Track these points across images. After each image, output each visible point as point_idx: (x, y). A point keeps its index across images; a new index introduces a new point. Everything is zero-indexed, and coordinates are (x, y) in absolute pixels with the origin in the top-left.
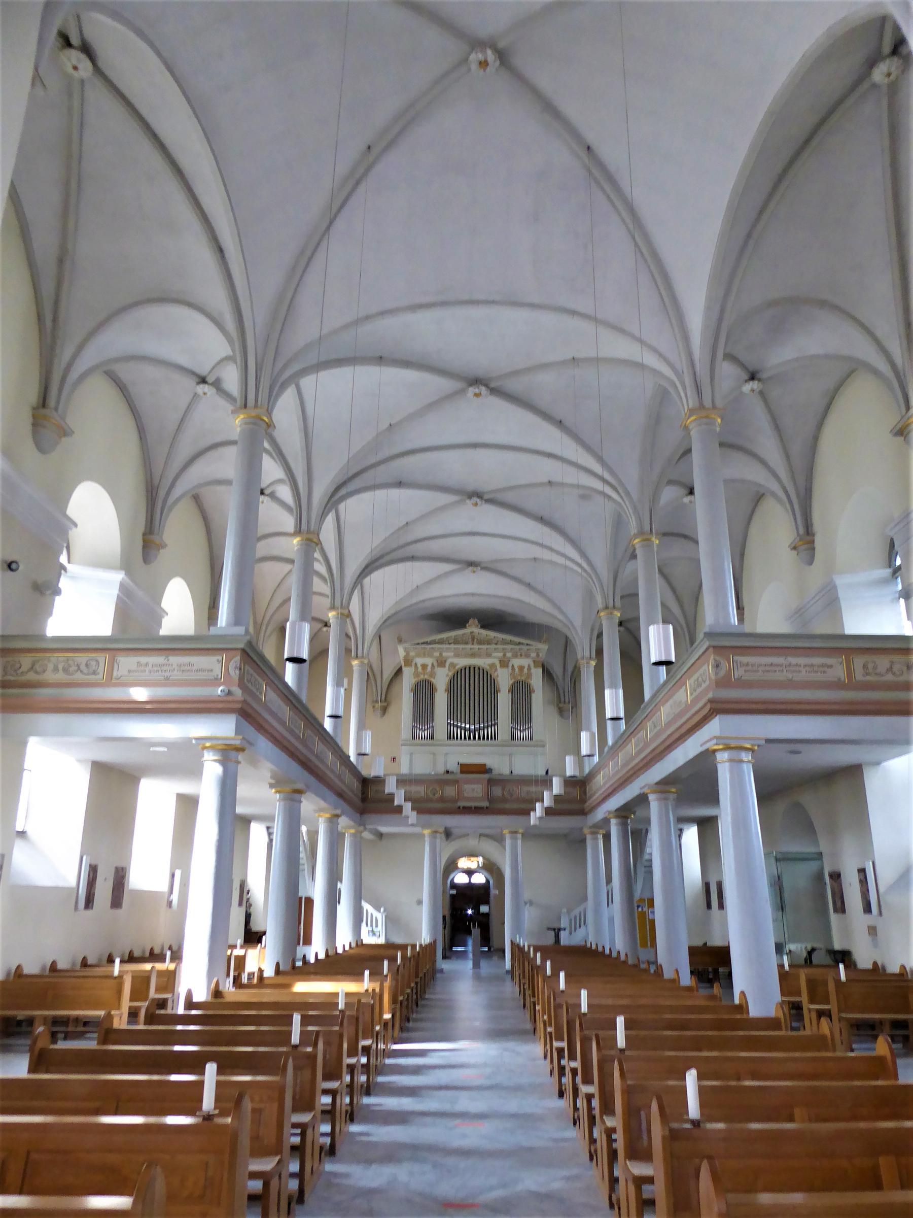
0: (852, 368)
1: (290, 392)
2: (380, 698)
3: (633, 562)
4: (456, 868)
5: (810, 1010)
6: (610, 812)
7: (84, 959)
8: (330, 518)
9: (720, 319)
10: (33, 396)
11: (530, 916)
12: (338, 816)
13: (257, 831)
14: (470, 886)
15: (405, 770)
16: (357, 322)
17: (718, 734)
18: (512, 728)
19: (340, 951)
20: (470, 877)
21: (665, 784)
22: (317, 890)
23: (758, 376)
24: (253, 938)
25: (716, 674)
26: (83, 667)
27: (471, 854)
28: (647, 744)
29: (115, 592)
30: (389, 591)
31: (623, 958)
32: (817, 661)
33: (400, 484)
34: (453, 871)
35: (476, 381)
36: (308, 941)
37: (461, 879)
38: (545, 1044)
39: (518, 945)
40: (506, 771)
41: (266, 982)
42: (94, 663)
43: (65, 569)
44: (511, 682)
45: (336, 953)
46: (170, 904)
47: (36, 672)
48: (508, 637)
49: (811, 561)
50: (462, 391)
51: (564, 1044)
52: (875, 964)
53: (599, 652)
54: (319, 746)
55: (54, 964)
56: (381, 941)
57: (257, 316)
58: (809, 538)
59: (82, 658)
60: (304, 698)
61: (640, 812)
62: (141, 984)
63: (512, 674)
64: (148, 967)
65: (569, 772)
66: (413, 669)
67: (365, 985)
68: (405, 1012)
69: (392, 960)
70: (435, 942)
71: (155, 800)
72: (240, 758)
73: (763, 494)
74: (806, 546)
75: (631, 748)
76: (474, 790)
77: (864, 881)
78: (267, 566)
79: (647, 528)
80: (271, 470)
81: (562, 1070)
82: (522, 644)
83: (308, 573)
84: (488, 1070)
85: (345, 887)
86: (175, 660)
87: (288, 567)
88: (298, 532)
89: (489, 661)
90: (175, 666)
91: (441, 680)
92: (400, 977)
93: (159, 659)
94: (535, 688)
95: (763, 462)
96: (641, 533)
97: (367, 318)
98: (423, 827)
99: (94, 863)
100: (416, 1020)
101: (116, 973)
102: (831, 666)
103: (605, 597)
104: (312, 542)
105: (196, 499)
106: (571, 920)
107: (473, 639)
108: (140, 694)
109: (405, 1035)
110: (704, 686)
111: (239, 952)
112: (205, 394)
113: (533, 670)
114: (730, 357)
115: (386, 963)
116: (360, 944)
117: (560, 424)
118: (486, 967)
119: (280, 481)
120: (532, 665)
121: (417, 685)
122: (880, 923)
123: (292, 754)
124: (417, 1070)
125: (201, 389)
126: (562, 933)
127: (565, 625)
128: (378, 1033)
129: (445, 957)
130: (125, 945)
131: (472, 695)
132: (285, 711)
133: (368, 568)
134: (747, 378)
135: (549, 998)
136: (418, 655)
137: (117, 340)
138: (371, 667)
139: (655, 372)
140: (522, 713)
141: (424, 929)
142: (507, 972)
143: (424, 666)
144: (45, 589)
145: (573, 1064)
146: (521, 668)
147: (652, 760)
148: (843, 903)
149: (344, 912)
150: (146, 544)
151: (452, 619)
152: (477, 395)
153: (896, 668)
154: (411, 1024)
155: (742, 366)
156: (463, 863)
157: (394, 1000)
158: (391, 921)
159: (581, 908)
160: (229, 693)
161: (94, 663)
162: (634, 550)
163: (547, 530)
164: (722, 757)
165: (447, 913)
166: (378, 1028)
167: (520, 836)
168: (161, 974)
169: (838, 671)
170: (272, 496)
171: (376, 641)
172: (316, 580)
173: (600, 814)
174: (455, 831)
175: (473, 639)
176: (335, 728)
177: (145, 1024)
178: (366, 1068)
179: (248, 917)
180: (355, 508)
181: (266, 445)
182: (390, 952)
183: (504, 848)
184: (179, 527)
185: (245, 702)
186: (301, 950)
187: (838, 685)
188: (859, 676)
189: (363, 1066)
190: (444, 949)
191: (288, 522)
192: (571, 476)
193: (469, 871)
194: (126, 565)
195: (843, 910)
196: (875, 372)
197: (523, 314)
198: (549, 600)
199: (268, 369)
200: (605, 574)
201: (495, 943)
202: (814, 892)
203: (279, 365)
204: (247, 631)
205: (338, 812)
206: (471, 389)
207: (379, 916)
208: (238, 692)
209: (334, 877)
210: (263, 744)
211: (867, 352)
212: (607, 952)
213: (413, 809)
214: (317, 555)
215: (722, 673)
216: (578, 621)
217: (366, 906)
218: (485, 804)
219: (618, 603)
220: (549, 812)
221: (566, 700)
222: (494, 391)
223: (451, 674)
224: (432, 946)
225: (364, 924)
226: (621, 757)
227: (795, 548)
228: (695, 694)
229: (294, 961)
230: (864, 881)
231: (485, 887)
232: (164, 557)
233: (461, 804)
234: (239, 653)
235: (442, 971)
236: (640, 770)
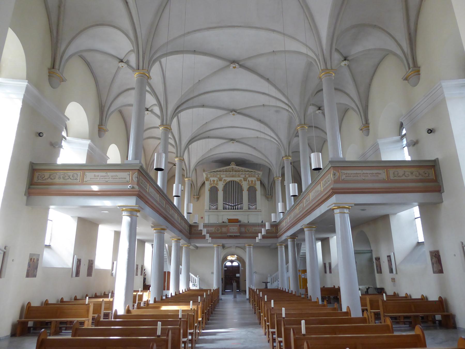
0: (387, 53)
1: (157, 65)
2: (196, 194)
3: (296, 138)
4: (227, 259)
5: (371, 312)
6: (288, 236)
7: (76, 296)
8: (175, 120)
9: (335, 29)
10: (48, 64)
11: (256, 278)
12: (180, 240)
13: (148, 247)
14: (232, 267)
15: (206, 222)
16: (184, 35)
17: (335, 202)
19: (181, 292)
20: (232, 263)
21: (311, 225)
22: (172, 269)
23: (348, 59)
24: (146, 287)
25: (334, 178)
26: (71, 177)
27: (232, 255)
28: (304, 209)
29: (87, 148)
30: (199, 151)
31: (294, 293)
32: (375, 171)
33: (203, 106)
34: (225, 261)
35: (234, 62)
36: (168, 289)
37: (229, 264)
38: (266, 329)
39: (252, 289)
40: (246, 221)
41: (150, 306)
42: (75, 175)
43: (65, 139)
44: (248, 187)
45: (180, 293)
46: (112, 274)
47: (51, 179)
48: (247, 169)
49: (368, 135)
50: (228, 66)
51: (275, 330)
52: (395, 293)
53: (283, 175)
54: (172, 212)
55: (62, 299)
56: (198, 288)
57: (143, 32)
58: (367, 125)
59: (70, 173)
60: (165, 192)
61: (300, 237)
62: (97, 308)
63: (249, 184)
64: (101, 300)
65: (273, 220)
66: (209, 182)
67: (191, 306)
68: (207, 317)
69: (202, 296)
70: (219, 288)
71: (105, 233)
72: (138, 214)
73: (348, 109)
75: (297, 211)
76: (234, 229)
78: (151, 141)
80: (150, 100)
81: (274, 340)
83: (166, 143)
84: (242, 341)
85: (183, 267)
86: (110, 174)
87: (158, 141)
88: (162, 124)
89: (239, 179)
90: (110, 177)
91: (220, 186)
92: (205, 303)
93: (103, 174)
95: (348, 95)
96: (300, 124)
97: (189, 33)
98: (214, 244)
99: (79, 258)
100: (212, 320)
101: (87, 303)
102: (380, 174)
103: (285, 152)
104: (167, 128)
105: (121, 112)
107: (233, 170)
108: (95, 188)
109: (207, 326)
110: (329, 183)
111: (140, 293)
112: (122, 67)
113: (257, 182)
114: (337, 50)
115: (199, 297)
116: (189, 290)
117: (268, 80)
118: (239, 298)
119: (155, 105)
121: (211, 188)
123: (160, 214)
124: (212, 341)
125: (121, 64)
126: (268, 284)
127: (269, 164)
128: (196, 326)
129: (222, 294)
130: (92, 292)
131: (233, 193)
132: (157, 197)
133: (191, 141)
134: (343, 59)
135: (267, 310)
136: (211, 177)
137: (83, 42)
138: (192, 181)
139: (307, 55)
140: (252, 199)
141: (214, 283)
142: (247, 299)
143: (214, 181)
144: (55, 146)
145: (280, 339)
146: (252, 181)
147: (305, 215)
149: (182, 278)
150: (99, 129)
151: (224, 162)
152: (234, 67)
154: (210, 321)
155: (341, 54)
156: (229, 258)
157: (203, 312)
158: (202, 280)
159: (275, 274)
160: (133, 188)
161: (75, 175)
162: (298, 132)
163: (262, 125)
164: (337, 211)
165: (223, 277)
166: (196, 324)
167: (252, 247)
168: (106, 303)
170: (152, 111)
171: (194, 172)
172: (170, 146)
173: (284, 237)
174: (226, 245)
175: (233, 170)
176: (178, 202)
178: (191, 341)
179: (145, 279)
180: (185, 115)
181: (148, 88)
182: (201, 293)
183: (246, 252)
184: (113, 123)
185: (139, 191)
186: (165, 292)
187: (383, 181)
189: (190, 340)
190: (222, 291)
191: (158, 122)
192: (273, 102)
193: (232, 261)
194: (91, 137)
196: (395, 54)
197: (252, 32)
199: (148, 54)
200: (285, 142)
201: (242, 288)
202: (370, 266)
203: (153, 52)
204: (140, 162)
205: (180, 238)
206: (232, 65)
207: (197, 279)
208: (137, 188)
209: (178, 263)
210: (148, 210)
211: (393, 47)
212: (287, 291)
213: (210, 237)
214: (170, 136)
215: (336, 177)
216: (274, 162)
217: (191, 275)
218: (239, 234)
219: (291, 154)
220: (264, 237)
221: (269, 194)
222: (241, 66)
223: (224, 184)
224: (218, 290)
225: (191, 282)
226: (292, 215)
227: (361, 130)
228: (325, 187)
229: (162, 297)
231: (238, 267)
232: (108, 135)
233: (229, 235)
234: (137, 171)
235: (221, 300)
236: (300, 219)
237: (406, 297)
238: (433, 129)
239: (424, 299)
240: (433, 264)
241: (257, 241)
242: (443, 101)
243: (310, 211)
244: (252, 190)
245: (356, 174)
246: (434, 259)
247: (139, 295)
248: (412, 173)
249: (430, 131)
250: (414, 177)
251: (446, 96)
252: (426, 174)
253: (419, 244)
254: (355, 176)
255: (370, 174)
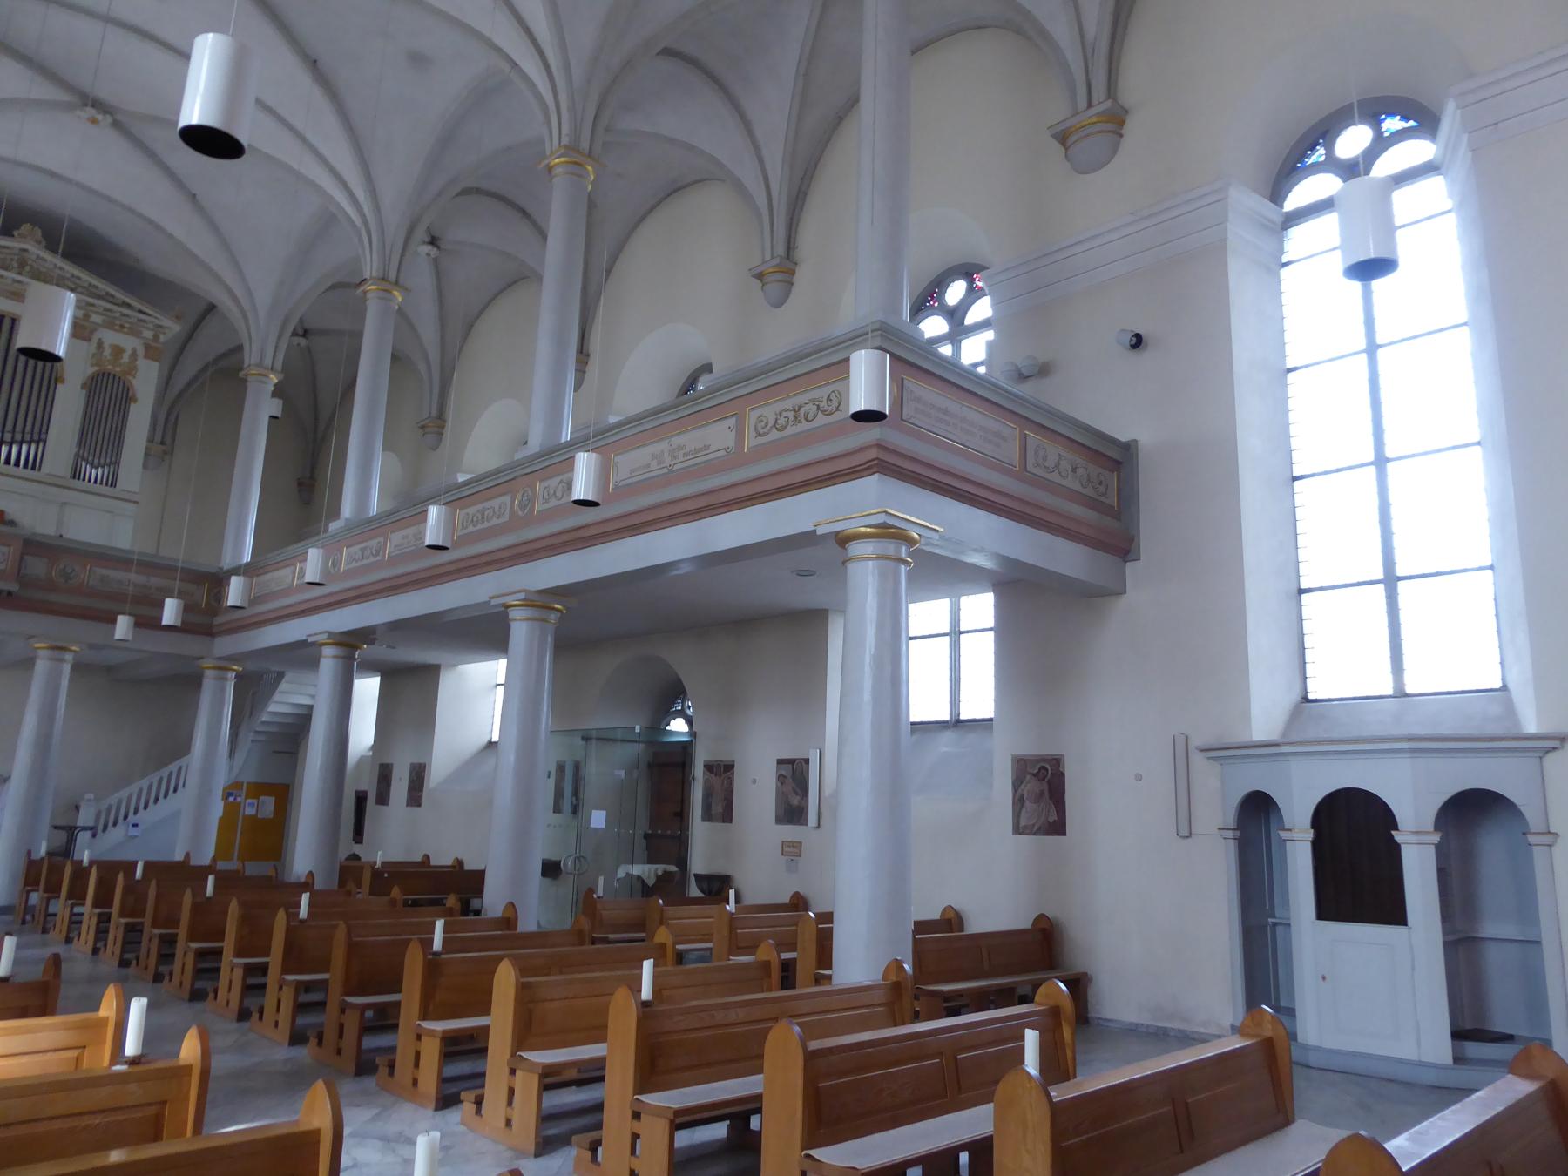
18: (77, 455)
74: (779, 276)
79: (585, 145)
82: (129, 306)
94: (139, 396)
106: (99, 814)
113: (142, 363)
120: (141, 351)
140: (101, 435)
146: (118, 351)
195: (727, 816)
198: (225, 244)
227: (760, 276)
241: (117, 636)
242: (1216, 253)
243: (584, 539)
244: (109, 394)
247: (228, 858)
250: (1077, 487)
251: (1230, 235)
253: (491, 744)
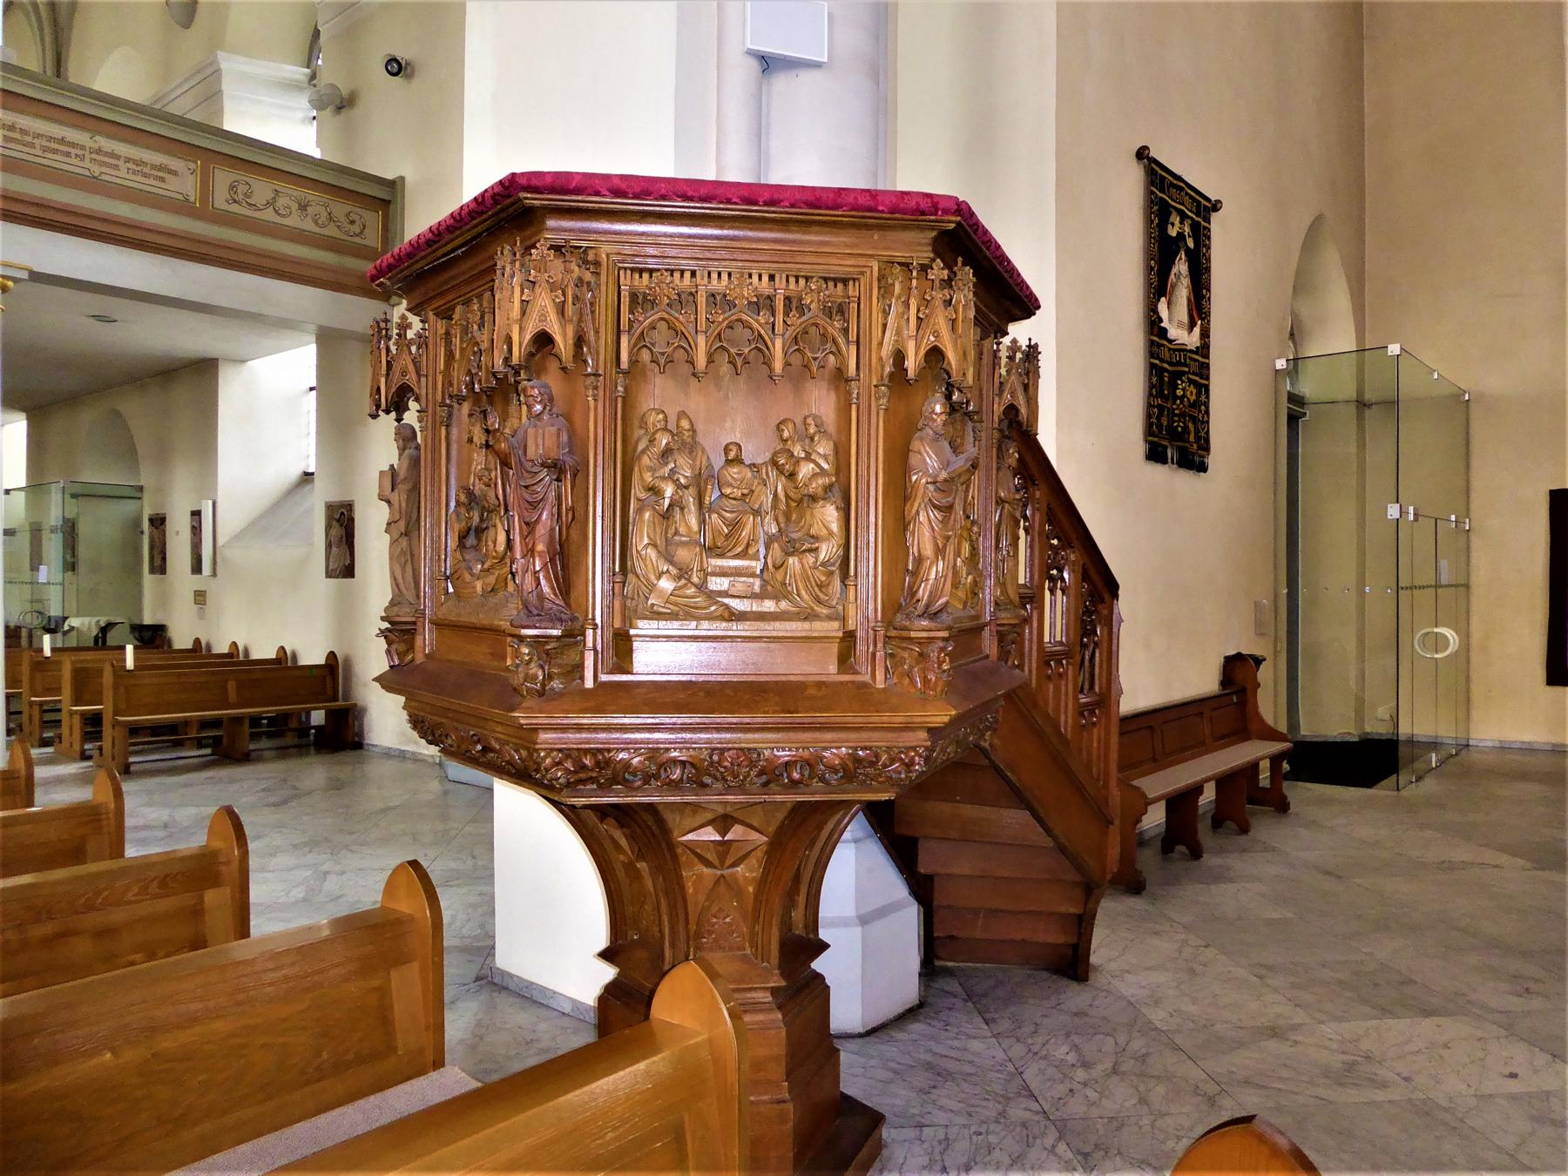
52: (197, 641)
77: (196, 530)
102: (175, 173)
122: (212, 587)
148: (164, 559)
153: (281, 202)
169: (185, 184)
177: (57, 690)
187: (182, 207)
188: (220, 200)
230: (196, 530)
237: (277, 661)
238: (407, 64)
239: (283, 663)
240: (329, 546)
245: (62, 141)
246: (337, 531)
248: (303, 207)
249: (396, 67)
252: (352, 222)
254: (55, 151)
255: (128, 160)
